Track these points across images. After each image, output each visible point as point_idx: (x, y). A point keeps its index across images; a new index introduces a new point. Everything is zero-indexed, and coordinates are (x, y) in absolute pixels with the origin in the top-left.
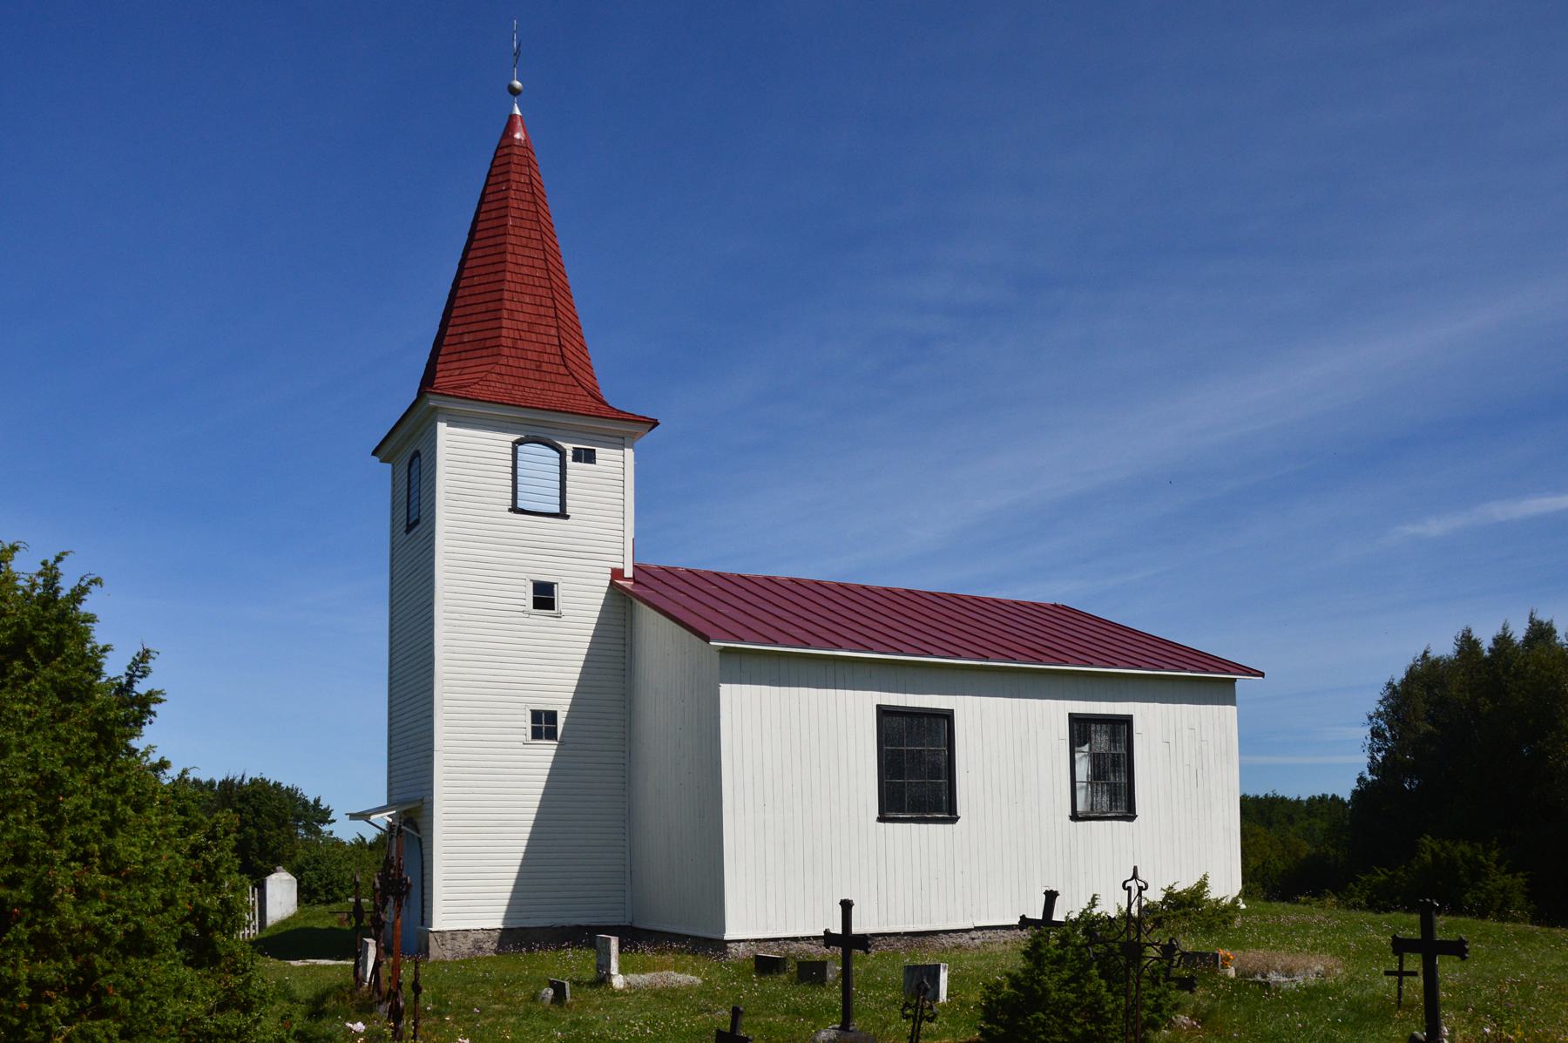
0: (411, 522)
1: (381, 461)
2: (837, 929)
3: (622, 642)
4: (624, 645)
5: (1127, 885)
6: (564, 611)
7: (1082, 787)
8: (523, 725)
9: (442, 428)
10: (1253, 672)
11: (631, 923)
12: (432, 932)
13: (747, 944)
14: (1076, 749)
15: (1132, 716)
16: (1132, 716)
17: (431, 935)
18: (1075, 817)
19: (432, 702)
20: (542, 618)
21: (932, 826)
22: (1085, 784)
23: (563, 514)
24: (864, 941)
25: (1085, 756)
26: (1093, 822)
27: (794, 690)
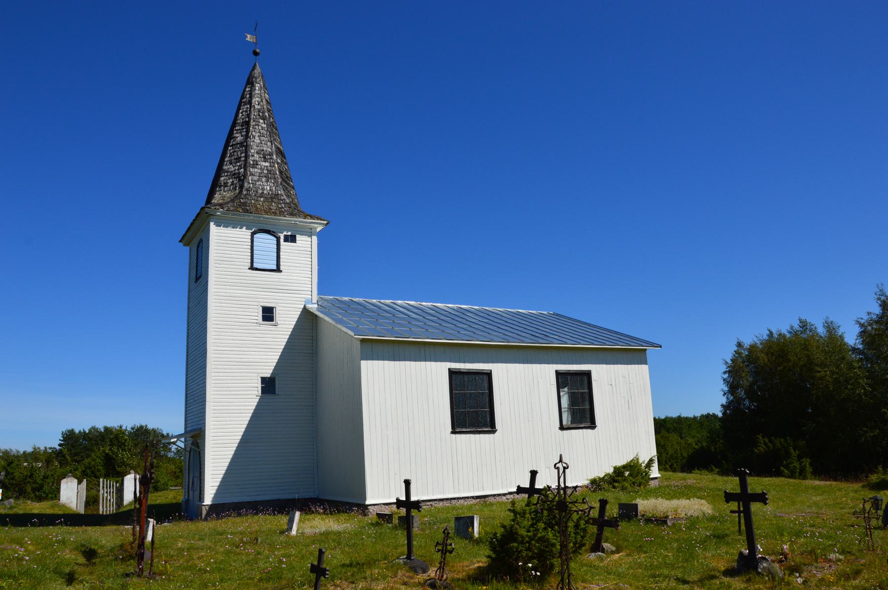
0: (198, 276)
1: (184, 245)
2: (403, 498)
3: (312, 338)
4: (313, 340)
5: (557, 466)
6: (279, 322)
7: (565, 411)
8: (256, 385)
9: (212, 225)
10: (655, 345)
11: (318, 496)
12: (204, 505)
13: (379, 506)
14: (561, 390)
15: (591, 371)
16: (591, 371)
17: (203, 507)
18: (562, 428)
19: (205, 375)
20: (267, 326)
21: (482, 436)
22: (567, 409)
23: (278, 270)
24: (417, 505)
25: (566, 393)
26: (572, 431)
27: (403, 363)
